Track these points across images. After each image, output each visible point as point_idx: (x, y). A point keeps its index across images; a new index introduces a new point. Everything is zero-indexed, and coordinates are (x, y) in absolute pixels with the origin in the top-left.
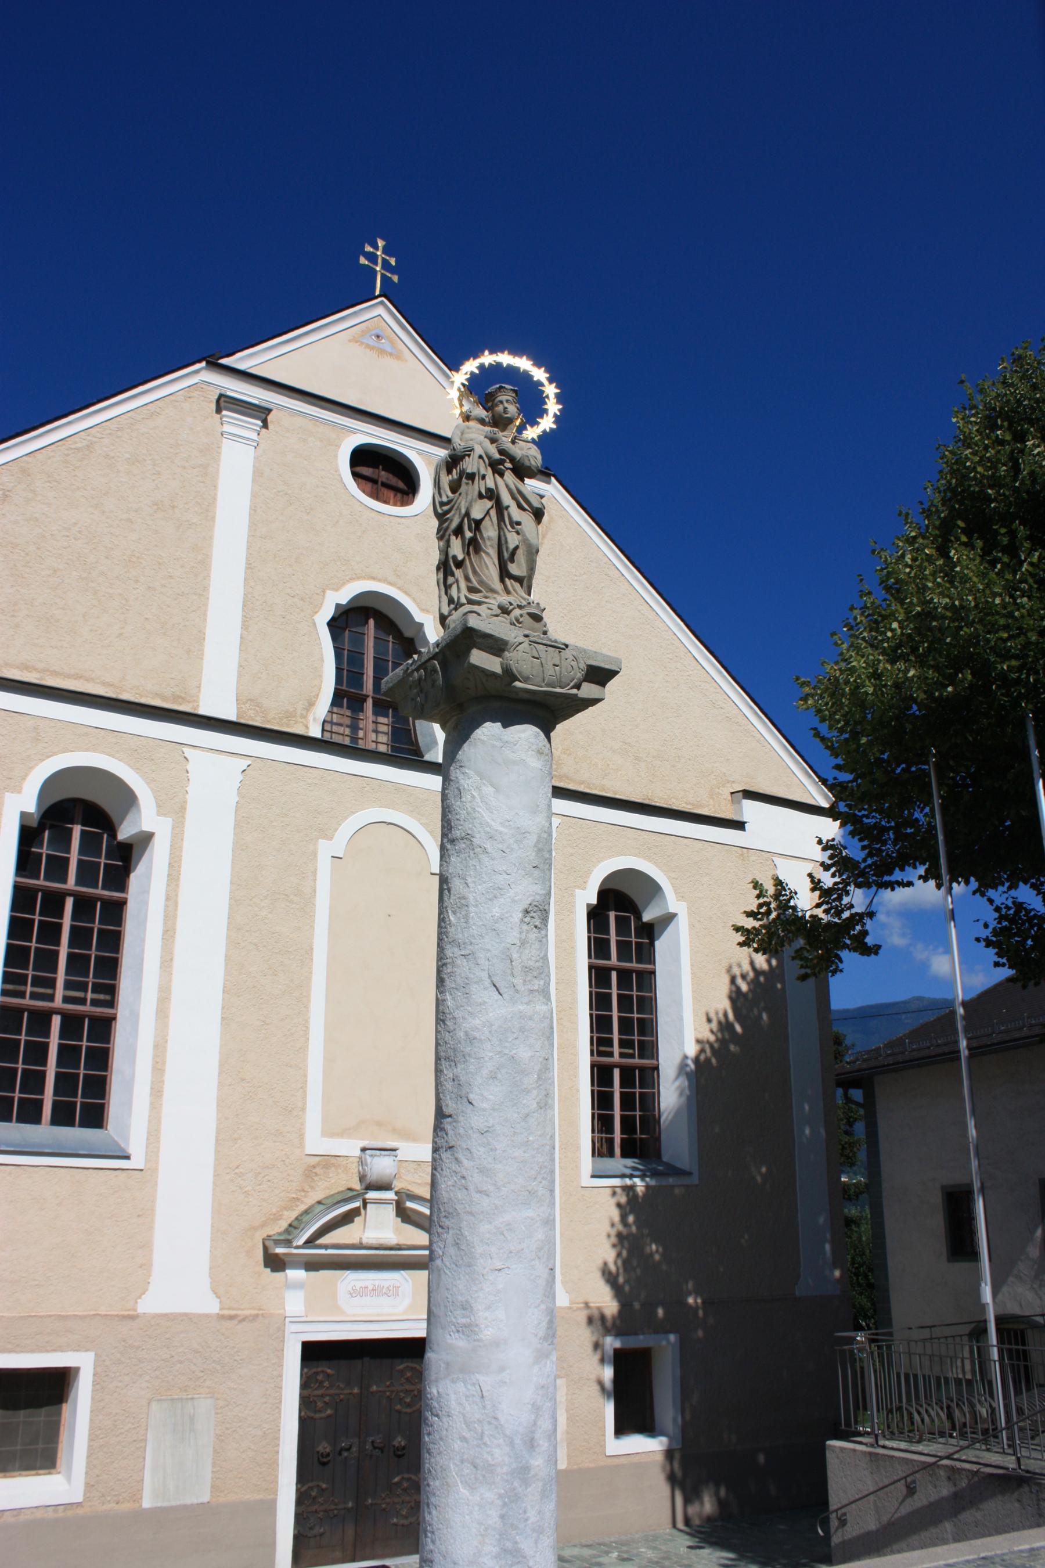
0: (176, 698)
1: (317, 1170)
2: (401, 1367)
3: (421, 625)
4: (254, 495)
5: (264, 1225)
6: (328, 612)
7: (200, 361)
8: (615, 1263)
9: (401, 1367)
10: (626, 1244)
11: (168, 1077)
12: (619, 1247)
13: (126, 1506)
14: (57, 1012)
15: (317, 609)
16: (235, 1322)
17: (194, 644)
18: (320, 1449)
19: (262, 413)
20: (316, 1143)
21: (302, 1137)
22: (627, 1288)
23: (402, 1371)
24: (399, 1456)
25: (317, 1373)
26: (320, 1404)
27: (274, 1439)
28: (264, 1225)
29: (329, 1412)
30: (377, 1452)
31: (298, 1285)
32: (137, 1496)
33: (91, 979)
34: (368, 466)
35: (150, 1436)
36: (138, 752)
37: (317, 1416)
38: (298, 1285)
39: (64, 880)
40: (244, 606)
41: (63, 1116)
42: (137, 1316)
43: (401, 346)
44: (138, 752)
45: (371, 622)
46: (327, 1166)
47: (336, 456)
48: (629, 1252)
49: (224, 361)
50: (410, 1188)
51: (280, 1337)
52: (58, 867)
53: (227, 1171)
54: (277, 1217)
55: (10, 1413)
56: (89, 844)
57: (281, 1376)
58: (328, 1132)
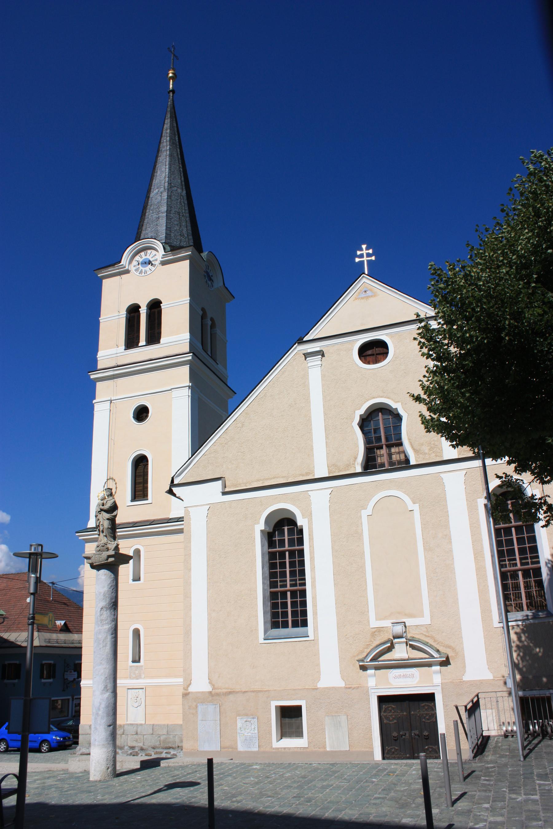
0: (307, 474)
1: (376, 633)
2: (423, 705)
3: (397, 409)
4: (323, 386)
5: (358, 655)
6: (357, 419)
7: (295, 344)
8: (517, 659)
9: (423, 705)
10: (522, 650)
11: (318, 607)
12: (518, 652)
13: (322, 750)
14: (289, 591)
15: (352, 420)
16: (351, 689)
17: (309, 452)
18: (393, 735)
19: (322, 353)
20: (374, 623)
21: (369, 622)
22: (524, 669)
23: (424, 706)
24: (426, 739)
25: (389, 707)
26: (391, 718)
27: (369, 729)
28: (358, 655)
29: (395, 721)
30: (417, 737)
31: (371, 676)
32: (324, 747)
33: (298, 578)
34: (370, 350)
35: (326, 728)
36: (292, 498)
37: (391, 723)
38: (435, 672)
39: (285, 547)
40: (325, 430)
41: (295, 624)
42: (317, 689)
43: (376, 290)
44: (292, 498)
45: (380, 414)
46: (379, 631)
47: (352, 354)
48: (524, 653)
49: (304, 339)
50: (414, 636)
52: (282, 543)
53: (342, 637)
54: (363, 652)
55: (290, 719)
56: (291, 532)
57: (369, 708)
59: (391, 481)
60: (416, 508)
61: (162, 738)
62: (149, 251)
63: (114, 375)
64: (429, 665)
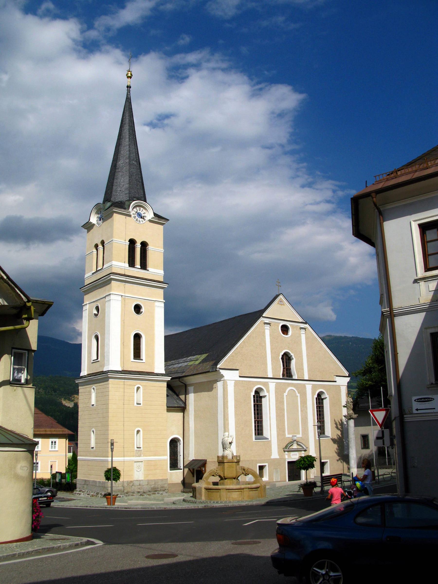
20: (287, 436)
38: (286, 454)
51: (285, 460)
58: (288, 434)
59: (293, 384)
60: (298, 395)
61: (152, 486)
62: (142, 209)
63: (125, 281)
64: (301, 451)
